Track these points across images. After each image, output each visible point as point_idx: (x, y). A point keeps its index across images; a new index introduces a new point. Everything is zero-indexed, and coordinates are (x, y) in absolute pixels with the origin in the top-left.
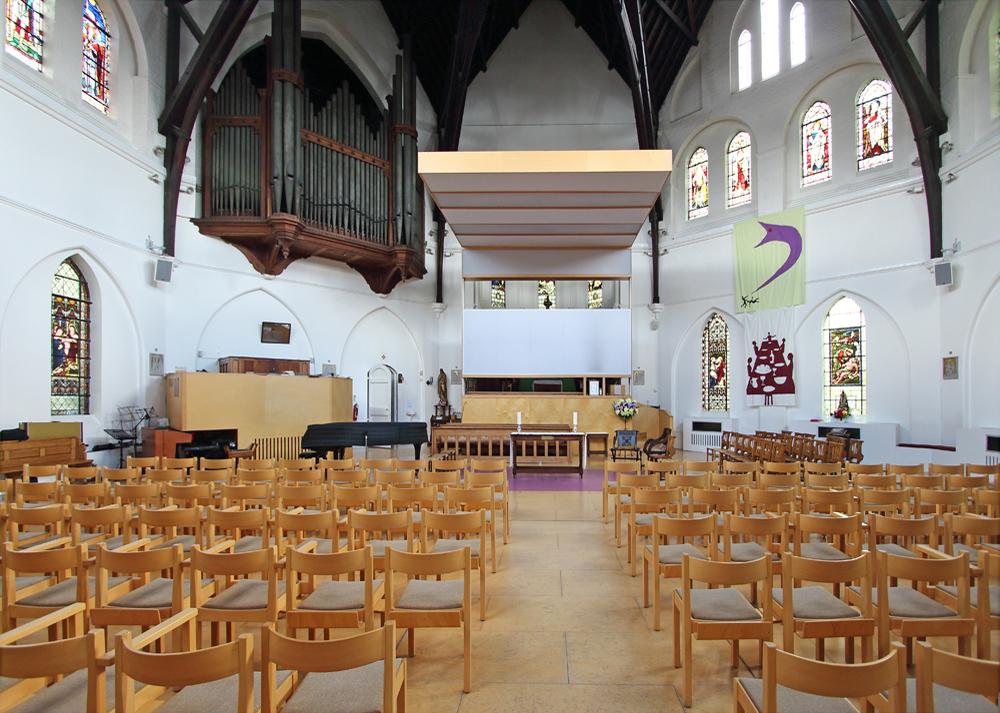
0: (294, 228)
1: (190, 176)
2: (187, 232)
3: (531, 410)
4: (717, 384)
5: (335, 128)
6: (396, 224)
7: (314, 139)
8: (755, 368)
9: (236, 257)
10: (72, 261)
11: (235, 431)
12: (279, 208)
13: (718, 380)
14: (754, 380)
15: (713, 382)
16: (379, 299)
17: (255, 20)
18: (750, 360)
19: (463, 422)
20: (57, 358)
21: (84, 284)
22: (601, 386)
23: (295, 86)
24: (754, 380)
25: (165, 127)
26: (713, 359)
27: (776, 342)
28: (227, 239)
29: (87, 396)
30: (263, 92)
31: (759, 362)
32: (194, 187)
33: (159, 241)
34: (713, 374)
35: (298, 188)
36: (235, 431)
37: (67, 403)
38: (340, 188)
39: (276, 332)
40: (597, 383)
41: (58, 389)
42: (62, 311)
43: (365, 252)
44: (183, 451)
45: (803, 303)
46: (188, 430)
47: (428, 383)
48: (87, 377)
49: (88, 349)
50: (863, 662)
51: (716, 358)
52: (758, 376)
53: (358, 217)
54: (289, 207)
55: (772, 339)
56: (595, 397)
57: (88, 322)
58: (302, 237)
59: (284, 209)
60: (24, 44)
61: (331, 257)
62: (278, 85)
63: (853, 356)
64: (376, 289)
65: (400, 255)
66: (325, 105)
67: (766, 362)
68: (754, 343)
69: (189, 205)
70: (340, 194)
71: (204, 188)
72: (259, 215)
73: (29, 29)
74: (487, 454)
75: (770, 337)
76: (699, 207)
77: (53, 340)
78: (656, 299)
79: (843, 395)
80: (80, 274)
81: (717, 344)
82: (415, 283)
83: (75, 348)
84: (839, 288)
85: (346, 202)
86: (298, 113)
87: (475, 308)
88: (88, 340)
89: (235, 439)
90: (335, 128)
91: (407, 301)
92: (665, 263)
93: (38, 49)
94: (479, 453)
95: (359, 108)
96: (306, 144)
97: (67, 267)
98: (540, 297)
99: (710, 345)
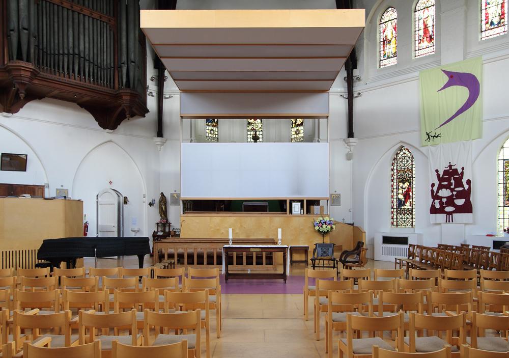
0: (29, 74)
3: (241, 226)
4: (404, 205)
8: (438, 192)
12: (25, 56)
13: (405, 202)
14: (437, 202)
15: (401, 203)
16: (106, 134)
18: (433, 185)
22: (302, 207)
26: (401, 184)
27: (456, 170)
31: (441, 187)
34: (401, 197)
35: (32, 39)
40: (299, 204)
45: (480, 137)
47: (150, 204)
51: (404, 183)
52: (440, 198)
53: (87, 64)
54: (25, 56)
55: (453, 168)
56: (297, 216)
58: (36, 82)
59: (20, 57)
67: (447, 187)
68: (437, 171)
70: (56, 47)
75: (450, 166)
78: (351, 134)
81: (405, 172)
87: (191, 141)
92: (358, 103)
99: (398, 172)
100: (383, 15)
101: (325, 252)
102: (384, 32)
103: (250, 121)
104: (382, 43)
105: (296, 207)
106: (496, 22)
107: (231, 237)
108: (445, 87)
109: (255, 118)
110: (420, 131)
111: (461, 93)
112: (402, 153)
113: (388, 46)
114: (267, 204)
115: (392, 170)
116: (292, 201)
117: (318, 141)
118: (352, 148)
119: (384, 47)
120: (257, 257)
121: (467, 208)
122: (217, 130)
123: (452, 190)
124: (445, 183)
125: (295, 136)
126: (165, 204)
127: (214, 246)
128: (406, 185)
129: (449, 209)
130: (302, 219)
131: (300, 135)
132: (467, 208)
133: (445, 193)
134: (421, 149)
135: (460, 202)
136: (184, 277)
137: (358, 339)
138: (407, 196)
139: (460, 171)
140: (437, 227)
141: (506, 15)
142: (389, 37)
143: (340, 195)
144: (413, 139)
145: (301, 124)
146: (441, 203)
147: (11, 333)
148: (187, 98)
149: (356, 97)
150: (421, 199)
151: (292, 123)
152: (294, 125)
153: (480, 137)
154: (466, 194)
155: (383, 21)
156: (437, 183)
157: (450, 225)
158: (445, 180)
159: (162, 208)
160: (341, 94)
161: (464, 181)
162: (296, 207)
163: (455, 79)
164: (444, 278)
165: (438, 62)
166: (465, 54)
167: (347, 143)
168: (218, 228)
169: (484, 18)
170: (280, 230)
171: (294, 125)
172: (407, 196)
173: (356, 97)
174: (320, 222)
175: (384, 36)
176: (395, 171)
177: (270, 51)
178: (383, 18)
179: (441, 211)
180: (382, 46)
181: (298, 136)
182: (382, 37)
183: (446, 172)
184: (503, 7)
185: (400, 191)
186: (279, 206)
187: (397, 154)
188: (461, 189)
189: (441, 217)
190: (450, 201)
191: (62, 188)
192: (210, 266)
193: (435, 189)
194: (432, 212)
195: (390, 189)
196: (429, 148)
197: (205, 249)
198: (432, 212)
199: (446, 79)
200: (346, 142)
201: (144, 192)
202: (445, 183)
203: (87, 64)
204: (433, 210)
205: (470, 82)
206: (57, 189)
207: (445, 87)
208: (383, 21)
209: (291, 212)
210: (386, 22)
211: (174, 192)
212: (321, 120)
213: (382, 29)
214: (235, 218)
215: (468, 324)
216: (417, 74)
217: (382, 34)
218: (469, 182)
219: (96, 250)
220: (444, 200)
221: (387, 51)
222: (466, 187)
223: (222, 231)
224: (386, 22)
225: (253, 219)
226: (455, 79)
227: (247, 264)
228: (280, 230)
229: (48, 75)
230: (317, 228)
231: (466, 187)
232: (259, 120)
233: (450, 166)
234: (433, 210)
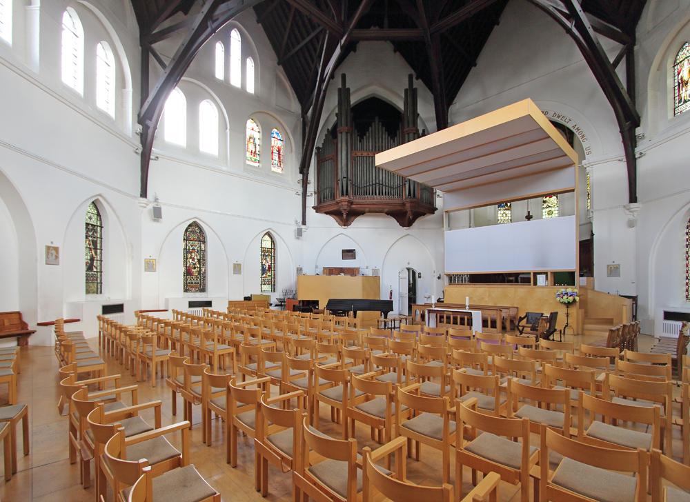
0: (346, 203)
1: (311, 188)
2: (311, 212)
3: (489, 295)
5: (371, 144)
6: (405, 187)
7: (359, 154)
9: (330, 220)
10: (268, 234)
11: (318, 301)
12: (345, 194)
16: (405, 230)
17: (335, 108)
19: (445, 302)
20: (264, 271)
21: (273, 242)
22: (547, 279)
23: (347, 133)
25: (301, 172)
28: (327, 213)
29: (274, 285)
30: (335, 141)
32: (313, 193)
33: (300, 220)
35: (349, 182)
36: (318, 301)
37: (267, 288)
38: (374, 175)
39: (349, 254)
40: (544, 276)
41: (263, 283)
42: (265, 253)
43: (388, 206)
44: (295, 309)
46: (601, 317)
47: (439, 278)
48: (274, 278)
49: (274, 267)
50: (133, 405)
53: (384, 187)
54: (345, 194)
56: (542, 287)
57: (274, 256)
58: (354, 206)
59: (343, 195)
60: (253, 158)
61: (375, 211)
62: (339, 135)
64: (402, 225)
65: (407, 205)
66: (365, 134)
69: (312, 201)
70: (374, 178)
71: (319, 192)
72: (347, 194)
73: (255, 152)
74: (457, 324)
76: (685, 102)
77: (262, 265)
78: (633, 199)
80: (271, 239)
82: (429, 217)
83: (270, 267)
84: (196, 216)
85: (377, 182)
86: (349, 145)
87: (470, 227)
88: (274, 263)
89: (318, 305)
90: (371, 144)
91: (424, 229)
92: (642, 166)
93: (258, 158)
94: (445, 322)
95: (384, 129)
96: (354, 159)
97: (267, 236)
98: (544, 211)
100: (677, 55)
102: (679, 74)
103: (545, 199)
104: (677, 88)
105: (541, 279)
107: (467, 304)
109: (550, 195)
113: (684, 89)
116: (535, 274)
118: (635, 214)
119: (679, 91)
120: (491, 322)
122: (510, 212)
136: (420, 333)
142: (686, 78)
143: (619, 265)
147: (649, 430)
148: (448, 196)
149: (639, 157)
155: (678, 61)
160: (620, 158)
167: (628, 209)
170: (467, 298)
173: (639, 157)
175: (680, 78)
177: (442, 162)
178: (678, 58)
180: (677, 91)
182: (676, 81)
200: (628, 208)
201: (434, 269)
203: (384, 187)
206: (608, 266)
208: (678, 61)
209: (535, 284)
210: (681, 62)
213: (676, 71)
217: (676, 77)
221: (683, 96)
224: (681, 62)
227: (447, 323)
228: (467, 298)
229: (361, 201)
232: (554, 197)
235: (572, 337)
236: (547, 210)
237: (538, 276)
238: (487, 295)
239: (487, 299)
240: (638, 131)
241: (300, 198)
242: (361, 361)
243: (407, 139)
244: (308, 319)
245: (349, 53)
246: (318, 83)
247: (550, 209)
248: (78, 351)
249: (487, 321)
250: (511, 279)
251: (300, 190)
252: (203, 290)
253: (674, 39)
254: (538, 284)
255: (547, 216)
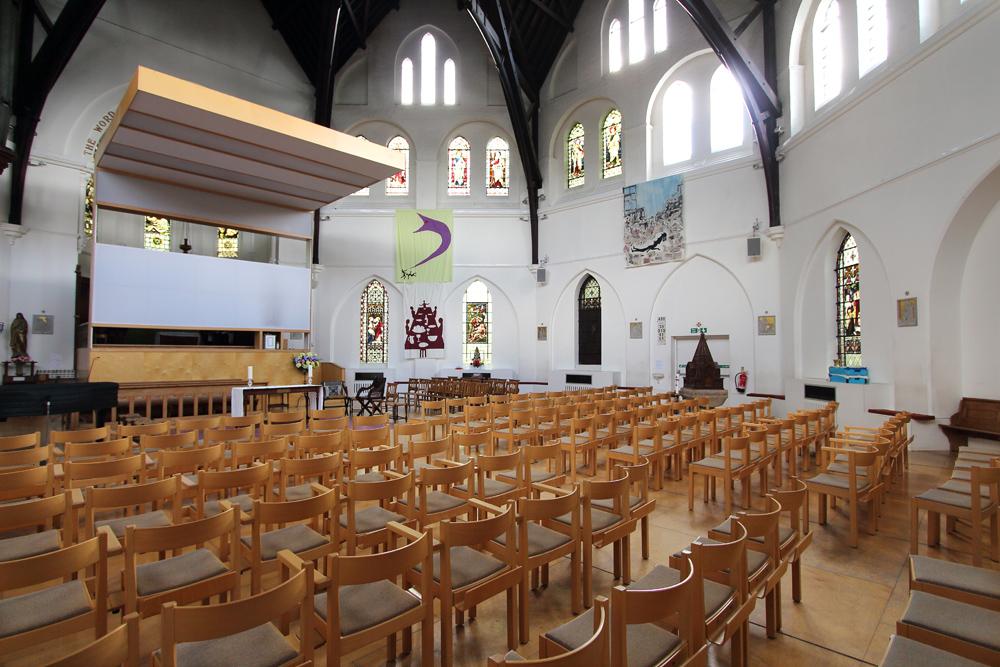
8: (412, 328)
13: (376, 337)
14: (412, 338)
15: (371, 338)
18: (408, 321)
24: (412, 338)
26: (371, 319)
31: (415, 324)
34: (372, 332)
50: (541, 658)
52: (415, 334)
56: (271, 351)
63: (483, 322)
67: (422, 324)
68: (412, 308)
75: (424, 305)
78: (316, 260)
79: (477, 350)
92: (324, 227)
101: (333, 391)
103: (149, 219)
106: (460, 183)
108: (420, 230)
109: (159, 217)
110: (396, 267)
111: (434, 239)
112: (373, 287)
114: (198, 335)
115: (362, 303)
116: (265, 333)
117: (277, 263)
120: (214, 404)
121: (439, 344)
123: (426, 327)
124: (420, 320)
125: (224, 250)
126: (25, 332)
127: (179, 391)
128: (377, 319)
129: (423, 345)
130: (278, 355)
131: (231, 249)
132: (439, 344)
133: (419, 329)
134: (397, 286)
135: (433, 338)
137: (41, 534)
138: (378, 330)
139: (433, 310)
140: (410, 362)
141: (468, 180)
144: (389, 275)
145: (235, 236)
146: (415, 339)
150: (396, 334)
151: (220, 233)
152: (222, 235)
153: (451, 280)
154: (438, 331)
156: (412, 320)
157: (424, 360)
158: (419, 317)
159: (18, 338)
161: (437, 319)
162: (270, 340)
163: (430, 224)
164: (266, 422)
165: (414, 205)
166: (437, 204)
168: (157, 367)
169: (450, 176)
170: (250, 368)
171: (222, 235)
172: (378, 330)
174: (303, 358)
176: (365, 304)
179: (415, 346)
181: (228, 250)
183: (420, 310)
184: (465, 172)
185: (371, 325)
186: (245, 339)
187: (368, 287)
188: (433, 326)
189: (415, 353)
190: (424, 337)
191: (908, 297)
192: (156, 420)
193: (410, 325)
194: (406, 348)
195: (359, 322)
196: (405, 285)
197: (165, 396)
198: (406, 348)
199: (421, 223)
202: (420, 320)
204: (408, 346)
205: (442, 229)
207: (420, 230)
209: (264, 347)
211: (41, 314)
212: (281, 239)
214: (185, 354)
215: (404, 454)
216: (393, 211)
218: (441, 320)
219: (49, 404)
220: (419, 336)
222: (439, 325)
223: (165, 371)
225: (213, 355)
226: (430, 224)
228: (250, 368)
230: (299, 365)
231: (439, 325)
233: (424, 305)
234: (408, 346)
235: (496, 405)
236: (154, 235)
237: (267, 337)
238: (191, 363)
239: (188, 371)
240: (540, 192)
241: (528, 225)
242: (150, 504)
243: (347, 130)
244: (300, 426)
245: (566, 36)
246: (509, 48)
247: (157, 235)
248: (965, 497)
249: (207, 404)
250: (103, 336)
251: (526, 211)
252: (244, 391)
253: (568, 118)
254: (267, 347)
255: (153, 245)
